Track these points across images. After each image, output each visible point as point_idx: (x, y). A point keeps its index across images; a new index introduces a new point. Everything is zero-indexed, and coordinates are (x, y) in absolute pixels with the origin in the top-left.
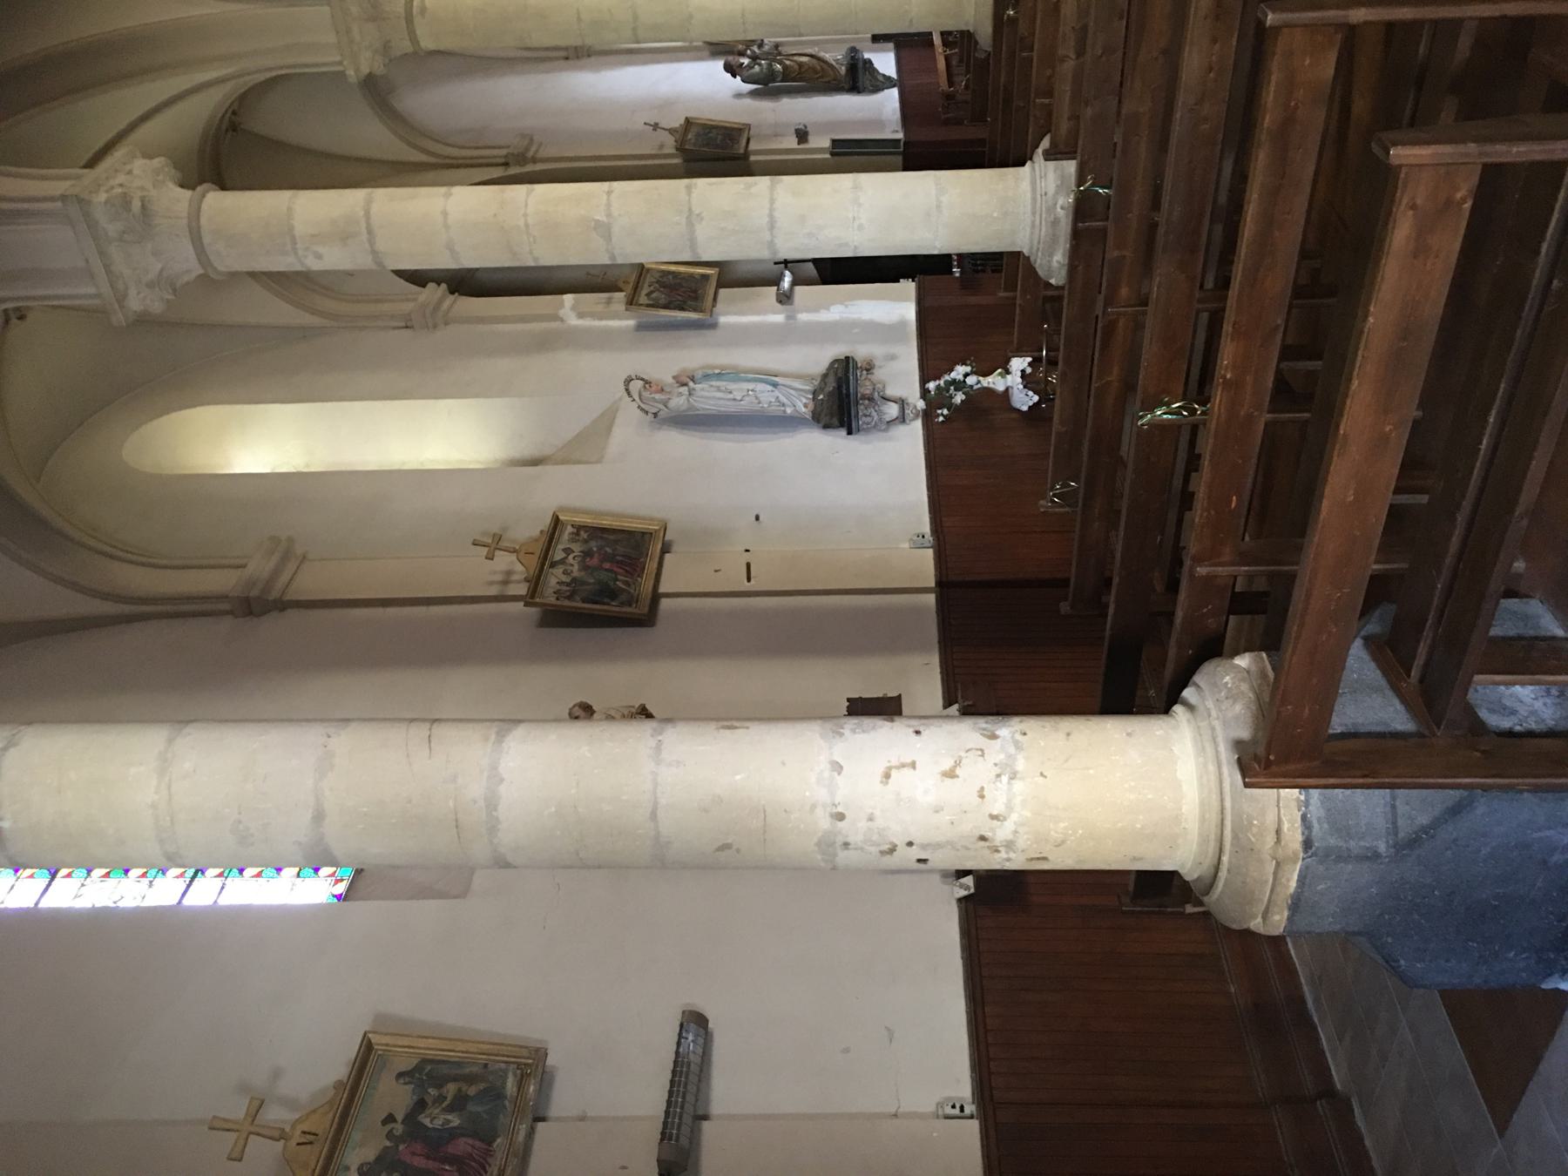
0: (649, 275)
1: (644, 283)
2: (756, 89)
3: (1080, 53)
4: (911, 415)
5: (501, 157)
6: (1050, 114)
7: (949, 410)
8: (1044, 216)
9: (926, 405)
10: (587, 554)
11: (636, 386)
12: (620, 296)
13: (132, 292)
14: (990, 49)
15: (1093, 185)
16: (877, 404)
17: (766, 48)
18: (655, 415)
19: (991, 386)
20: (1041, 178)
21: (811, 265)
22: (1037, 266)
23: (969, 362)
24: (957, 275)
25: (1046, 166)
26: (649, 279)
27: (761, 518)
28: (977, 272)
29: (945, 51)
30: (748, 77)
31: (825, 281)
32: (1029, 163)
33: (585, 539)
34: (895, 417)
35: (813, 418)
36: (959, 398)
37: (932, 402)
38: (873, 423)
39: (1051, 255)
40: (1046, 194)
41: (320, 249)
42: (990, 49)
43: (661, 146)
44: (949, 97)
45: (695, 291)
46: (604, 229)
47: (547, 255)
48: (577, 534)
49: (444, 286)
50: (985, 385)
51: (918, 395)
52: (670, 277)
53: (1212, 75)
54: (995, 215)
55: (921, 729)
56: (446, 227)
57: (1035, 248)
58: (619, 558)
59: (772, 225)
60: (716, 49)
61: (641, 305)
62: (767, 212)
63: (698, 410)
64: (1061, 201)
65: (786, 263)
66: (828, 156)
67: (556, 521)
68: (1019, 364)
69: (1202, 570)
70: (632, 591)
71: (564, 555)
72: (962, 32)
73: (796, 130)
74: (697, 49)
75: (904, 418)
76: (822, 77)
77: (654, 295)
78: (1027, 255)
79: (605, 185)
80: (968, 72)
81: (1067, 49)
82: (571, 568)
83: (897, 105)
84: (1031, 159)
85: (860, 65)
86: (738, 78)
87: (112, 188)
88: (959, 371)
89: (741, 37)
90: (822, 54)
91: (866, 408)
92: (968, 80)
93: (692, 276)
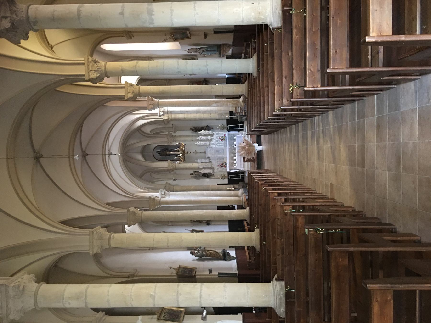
0: (165, 310)
1: (163, 313)
3: (283, 254)
5: (127, 275)
6: (276, 269)
8: (277, 297)
12: (156, 317)
13: (12, 313)
14: (260, 251)
17: (202, 249)
20: (275, 286)
21: (212, 308)
24: (254, 313)
25: (276, 283)
26: (165, 311)
28: (260, 312)
30: (197, 255)
31: (216, 313)
32: (272, 282)
39: (280, 308)
41: (70, 301)
42: (260, 251)
43: (172, 273)
44: (250, 262)
45: (178, 316)
46: (153, 297)
47: (136, 304)
49: (104, 312)
52: (171, 311)
53: (317, 261)
54: (264, 296)
56: (108, 295)
57: (275, 307)
59: (201, 297)
60: (188, 248)
61: (161, 320)
62: (200, 293)
64: (281, 293)
65: (205, 308)
66: (217, 277)
72: (252, 247)
73: (209, 270)
74: (184, 248)
76: (216, 256)
77: (165, 317)
78: (273, 308)
79: (155, 284)
80: (254, 257)
81: (279, 253)
83: (236, 264)
84: (272, 281)
85: (226, 253)
87: (16, 282)
89: (195, 246)
90: (216, 250)
92: (254, 259)
93: (177, 311)
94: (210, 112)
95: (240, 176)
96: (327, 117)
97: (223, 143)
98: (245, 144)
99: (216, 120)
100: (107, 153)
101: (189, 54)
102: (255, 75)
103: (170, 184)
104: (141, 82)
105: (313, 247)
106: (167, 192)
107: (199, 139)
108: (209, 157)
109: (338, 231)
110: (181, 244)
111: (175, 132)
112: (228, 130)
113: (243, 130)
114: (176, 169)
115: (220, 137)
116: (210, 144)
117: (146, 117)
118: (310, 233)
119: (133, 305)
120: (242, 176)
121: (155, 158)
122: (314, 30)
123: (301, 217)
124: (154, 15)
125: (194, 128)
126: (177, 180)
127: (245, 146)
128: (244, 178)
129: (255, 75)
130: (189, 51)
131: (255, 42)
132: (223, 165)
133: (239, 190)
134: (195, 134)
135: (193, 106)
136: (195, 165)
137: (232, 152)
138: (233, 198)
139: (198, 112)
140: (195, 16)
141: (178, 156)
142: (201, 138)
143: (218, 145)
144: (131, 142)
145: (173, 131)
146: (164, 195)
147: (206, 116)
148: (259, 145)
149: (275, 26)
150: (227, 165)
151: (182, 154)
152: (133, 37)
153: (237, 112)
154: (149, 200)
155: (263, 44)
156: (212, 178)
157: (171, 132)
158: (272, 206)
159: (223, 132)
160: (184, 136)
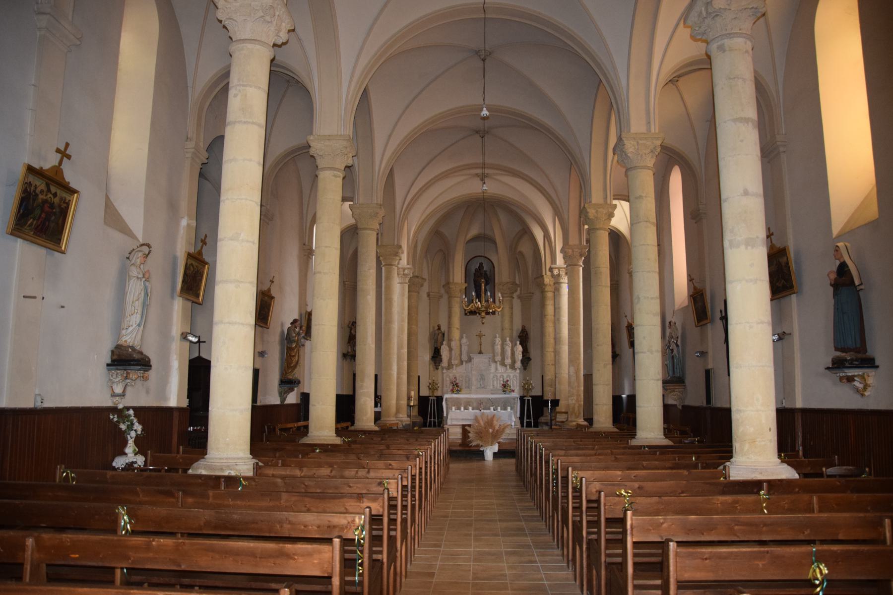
2: (284, 335)
4: (115, 400)
7: (116, 421)
9: (120, 409)
10: (52, 206)
11: (145, 249)
15: (243, 485)
16: (123, 381)
18: (128, 258)
19: (129, 445)
20: (245, 462)
22: (199, 462)
23: (143, 433)
25: (250, 464)
27: (62, 309)
29: (295, 427)
32: (251, 457)
33: (61, 206)
34: (115, 391)
36: (123, 427)
37: (120, 413)
38: (112, 379)
39: (205, 468)
40: (236, 465)
45: (191, 290)
48: (64, 202)
51: (126, 405)
52: (200, 278)
53: (303, 527)
58: (47, 223)
61: (187, 259)
63: (129, 282)
67: (73, 192)
68: (119, 462)
69: (30, 542)
70: (25, 227)
77: (191, 267)
85: (292, 386)
86: (290, 326)
88: (138, 427)
91: (121, 375)
93: (200, 289)
94: (557, 363)
95: (434, 418)
96: (561, 569)
97: (498, 387)
98: (497, 427)
99: (541, 375)
100: (487, 171)
101: (667, 324)
103: (422, 285)
104: (616, 237)
105: (329, 521)
106: (407, 280)
108: (472, 360)
109: (359, 570)
110: (318, 298)
111: (519, 297)
112: (522, 399)
114: (450, 298)
115: (508, 383)
116: (496, 362)
118: (356, 516)
119: (224, 202)
120: (435, 422)
121: (471, 259)
122: (736, 527)
123: (379, 507)
124: (746, 248)
125: (527, 334)
126: (429, 299)
127: (495, 428)
128: (430, 426)
130: (672, 323)
131: (692, 443)
132: (456, 387)
133: (409, 416)
134: (516, 334)
135: (569, 330)
136: (456, 334)
137: (480, 405)
138: (394, 402)
139: (557, 340)
141: (477, 300)
142: (507, 345)
144: (503, 216)
145: (521, 294)
146: (402, 273)
147: (549, 356)
148: (495, 454)
149: (730, 472)
150: (456, 394)
151: (480, 306)
152: (696, 223)
153: (558, 414)
154: (395, 244)
156: (431, 366)
157: (519, 289)
158: (390, 465)
159: (518, 388)
160: (512, 313)
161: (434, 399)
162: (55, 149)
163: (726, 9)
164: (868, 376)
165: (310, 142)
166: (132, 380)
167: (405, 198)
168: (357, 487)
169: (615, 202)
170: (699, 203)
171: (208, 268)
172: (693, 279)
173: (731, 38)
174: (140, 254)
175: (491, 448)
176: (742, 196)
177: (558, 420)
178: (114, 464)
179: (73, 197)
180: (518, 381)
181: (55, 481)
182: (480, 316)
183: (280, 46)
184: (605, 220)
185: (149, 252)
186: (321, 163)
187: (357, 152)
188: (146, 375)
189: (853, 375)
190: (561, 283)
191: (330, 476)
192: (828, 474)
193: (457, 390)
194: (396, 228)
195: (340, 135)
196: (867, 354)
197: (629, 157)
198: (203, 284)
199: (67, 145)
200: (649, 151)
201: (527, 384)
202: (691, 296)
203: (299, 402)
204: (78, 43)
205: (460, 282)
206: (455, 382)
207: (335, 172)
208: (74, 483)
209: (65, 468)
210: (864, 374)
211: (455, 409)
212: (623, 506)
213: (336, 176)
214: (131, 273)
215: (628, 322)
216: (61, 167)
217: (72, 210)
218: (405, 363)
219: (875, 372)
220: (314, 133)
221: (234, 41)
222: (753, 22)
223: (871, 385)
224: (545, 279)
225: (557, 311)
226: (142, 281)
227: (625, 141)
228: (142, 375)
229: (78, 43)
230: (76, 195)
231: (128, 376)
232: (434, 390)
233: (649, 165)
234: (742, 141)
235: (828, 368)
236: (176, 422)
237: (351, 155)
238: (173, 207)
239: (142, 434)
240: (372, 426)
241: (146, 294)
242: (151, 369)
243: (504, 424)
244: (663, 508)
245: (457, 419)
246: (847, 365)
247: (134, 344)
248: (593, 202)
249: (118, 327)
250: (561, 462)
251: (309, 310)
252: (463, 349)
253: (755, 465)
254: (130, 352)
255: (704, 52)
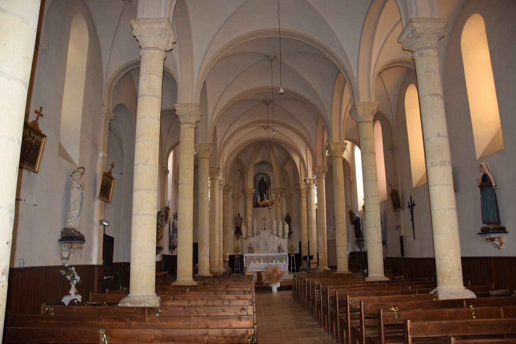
4: (63, 262)
7: (64, 274)
9: (66, 267)
10: (31, 145)
11: (82, 170)
16: (69, 250)
19: (72, 289)
23: (80, 281)
29: (160, 275)
32: (156, 295)
35: (65, 228)
36: (69, 278)
38: (62, 248)
39: (130, 303)
40: (149, 300)
48: (38, 143)
50: (72, 287)
55: (8, 244)
57: (131, 298)
63: (72, 190)
67: (43, 136)
68: (66, 300)
71: (32, 136)
75: (62, 259)
77: (105, 181)
82: (28, 138)
88: (78, 278)
93: (109, 194)
94: (309, 234)
95: (238, 268)
97: (275, 249)
98: (279, 273)
102: (368, 279)
106: (222, 188)
107: (279, 222)
108: (260, 234)
112: (289, 255)
113: (290, 271)
115: (281, 247)
117: (303, 165)
119: (138, 142)
120: (238, 271)
121: (257, 175)
122: (469, 327)
124: (441, 167)
126: (233, 199)
127: (278, 272)
129: (368, 279)
131: (400, 278)
132: (251, 250)
133: (224, 267)
134: (284, 218)
136: (250, 219)
137: (267, 259)
140: (443, 209)
143: (272, 243)
144: (276, 151)
145: (286, 195)
149: (439, 295)
150: (251, 253)
151: (268, 202)
152: (391, 153)
155: (409, 284)
156: (235, 238)
159: (287, 249)
161: (238, 257)
162: (35, 111)
163: (423, 33)
164: (503, 238)
165: (175, 107)
166: (74, 249)
167: (223, 139)
168: (229, 311)
169: (346, 141)
170: (393, 141)
171: (114, 182)
172: (391, 185)
173: (426, 49)
174: (79, 173)
175: (276, 285)
176: (437, 137)
177: (311, 267)
178: (63, 301)
179: (43, 139)
180: (287, 245)
181: (40, 313)
182: (268, 208)
183: (168, 52)
184: (341, 151)
185: (84, 172)
186: (182, 120)
187: (202, 114)
188: (82, 246)
189: (494, 237)
190: (311, 188)
191: (206, 305)
192: (493, 294)
193: (252, 252)
194: (217, 156)
195: (194, 104)
196: (501, 225)
197: (359, 116)
198: (111, 191)
199: (41, 108)
200: (371, 112)
201: (292, 247)
202: (390, 194)
203: (161, 260)
204: (47, 48)
205: (252, 188)
206: (250, 246)
207: (190, 125)
208: (53, 314)
209: (47, 305)
210: (500, 236)
211: (258, 263)
212: (393, 317)
213: (191, 127)
214: (73, 185)
215: (350, 210)
216: (38, 121)
217: (42, 147)
218: (222, 236)
219: (506, 235)
220: (178, 102)
221: (143, 49)
222: (438, 40)
223: (504, 242)
224: (301, 186)
225: (309, 204)
226: (80, 189)
227: (357, 107)
228: (80, 246)
229: (47, 48)
230: (45, 138)
231: (72, 246)
232: (238, 251)
233: (370, 120)
234: (435, 106)
235: (479, 234)
236: (96, 274)
237: (199, 115)
238: (95, 145)
239: (80, 282)
240: (208, 273)
241: (82, 197)
242: (85, 242)
243: (283, 271)
244: (416, 318)
245: (254, 269)
246: (491, 231)
247: (75, 227)
248: (334, 141)
249: (66, 216)
250: (338, 293)
251: (166, 206)
252: (254, 227)
253: (452, 290)
254: (73, 232)
255: (411, 58)
